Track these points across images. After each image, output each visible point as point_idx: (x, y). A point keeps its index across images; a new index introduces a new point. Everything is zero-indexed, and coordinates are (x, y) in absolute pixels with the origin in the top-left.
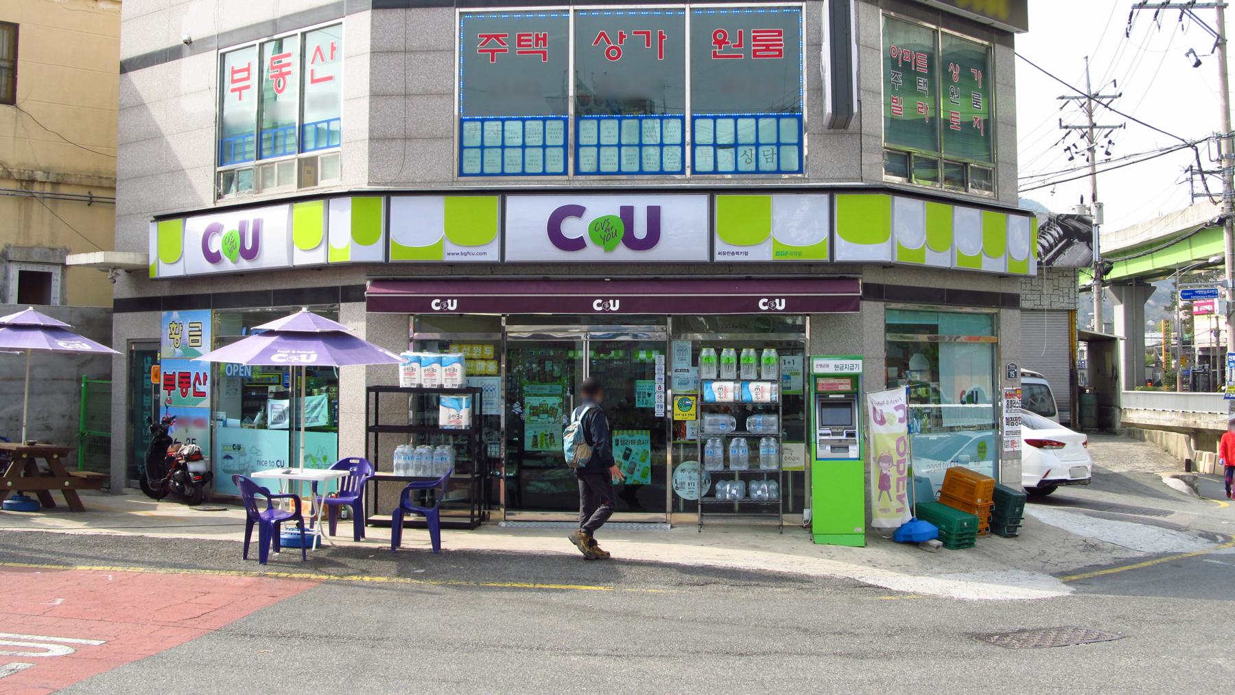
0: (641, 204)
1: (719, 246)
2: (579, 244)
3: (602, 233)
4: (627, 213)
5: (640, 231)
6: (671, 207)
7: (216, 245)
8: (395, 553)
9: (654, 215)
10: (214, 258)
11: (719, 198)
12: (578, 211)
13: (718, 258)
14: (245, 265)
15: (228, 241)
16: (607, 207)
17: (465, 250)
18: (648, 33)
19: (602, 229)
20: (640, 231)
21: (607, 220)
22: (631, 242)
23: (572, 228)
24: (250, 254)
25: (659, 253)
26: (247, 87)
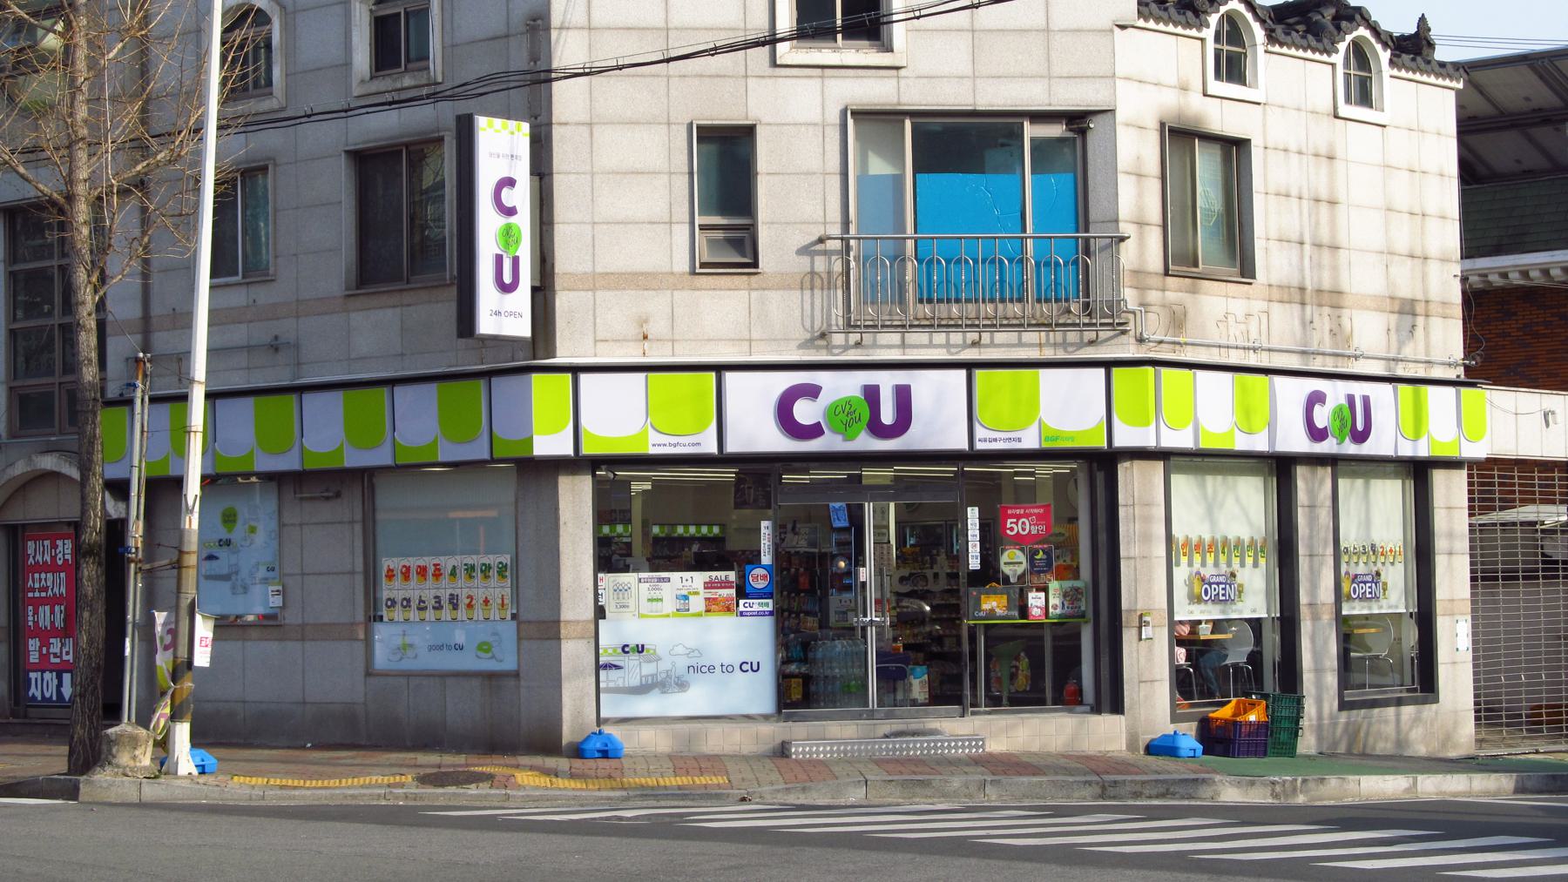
0: (887, 381)
1: (980, 432)
2: (815, 431)
3: (843, 417)
4: (872, 394)
5: (887, 416)
6: (923, 385)
7: (1322, 417)
8: (846, 744)
9: (903, 397)
10: (1317, 434)
11: (1116, 371)
12: (812, 392)
13: (979, 446)
14: (1351, 449)
15: (1338, 412)
16: (848, 385)
17: (674, 440)
18: (1205, 95)
19: (842, 414)
20: (887, 416)
21: (849, 402)
22: (877, 428)
23: (804, 412)
24: (1361, 437)
25: (915, 439)
26: (1366, 401)
